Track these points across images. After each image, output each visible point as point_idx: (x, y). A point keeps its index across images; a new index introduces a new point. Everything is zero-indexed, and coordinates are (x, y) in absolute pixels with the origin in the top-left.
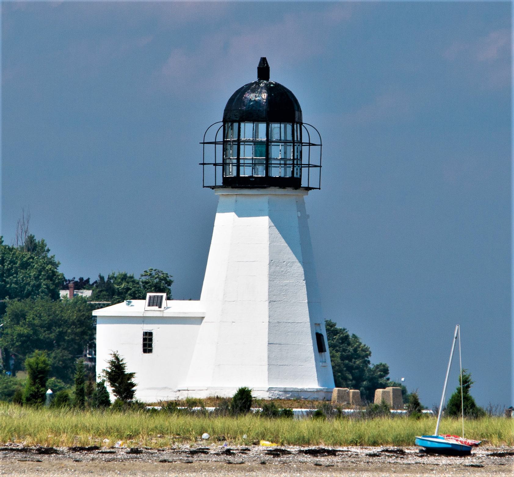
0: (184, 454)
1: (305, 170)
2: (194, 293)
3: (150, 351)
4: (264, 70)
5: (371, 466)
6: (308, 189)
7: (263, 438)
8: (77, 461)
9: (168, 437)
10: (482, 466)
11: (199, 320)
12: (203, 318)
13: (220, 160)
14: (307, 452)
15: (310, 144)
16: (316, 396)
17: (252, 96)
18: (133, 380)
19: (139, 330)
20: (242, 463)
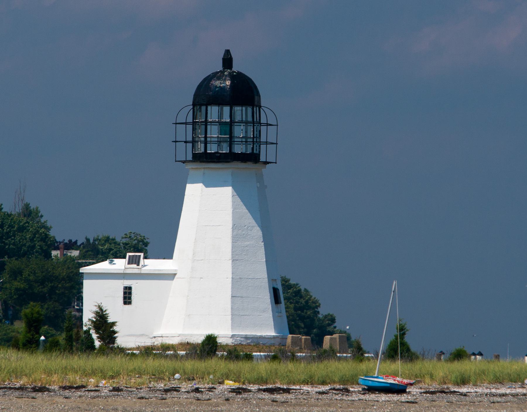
0: (159, 392)
4: (228, 61)
5: (320, 403)
6: (266, 163)
8: (66, 398)
9: (145, 377)
10: (416, 403)
11: (171, 276)
12: (175, 274)
13: (190, 139)
14: (265, 390)
15: (268, 125)
17: (217, 83)
18: (115, 328)
19: (119, 285)
20: (209, 400)
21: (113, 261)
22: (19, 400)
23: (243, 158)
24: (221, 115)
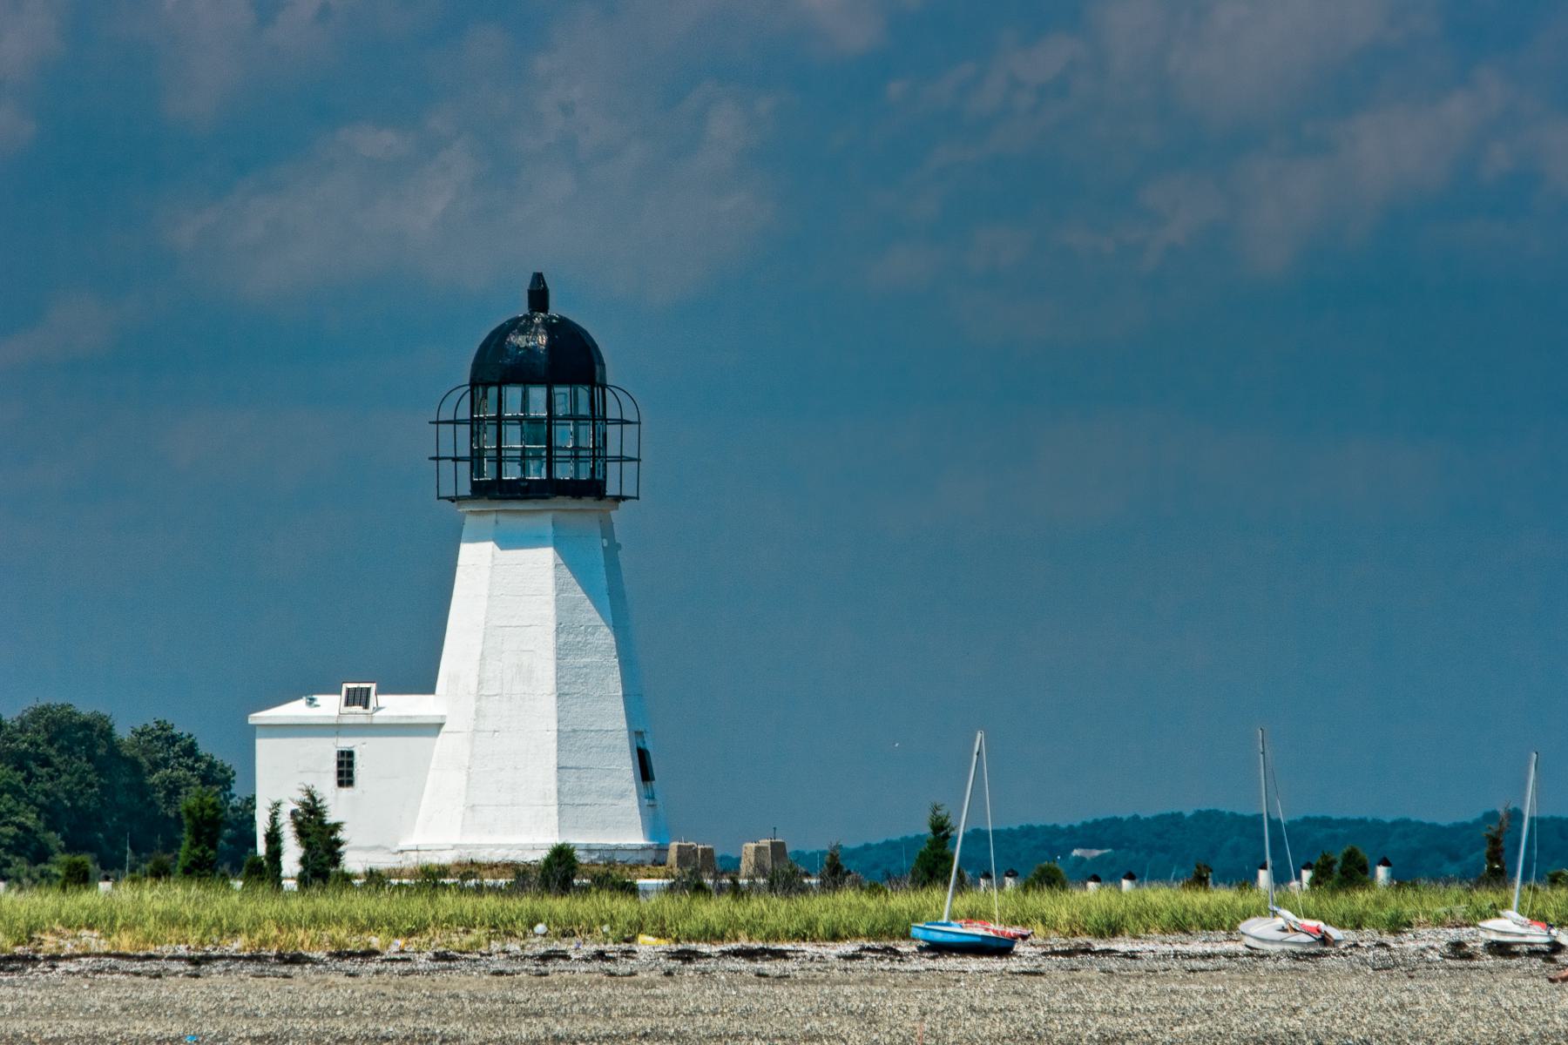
0: (528, 961)
1: (613, 468)
2: (425, 683)
3: (350, 783)
4: (539, 296)
5: (853, 977)
6: (620, 498)
7: (641, 929)
8: (351, 975)
9: (478, 933)
10: (1042, 974)
11: (433, 728)
12: (441, 725)
13: (464, 451)
14: (736, 953)
15: (622, 422)
16: (640, 857)
17: (520, 340)
18: (340, 835)
19: (326, 750)
20: (632, 974)
21: (312, 700)
22: (260, 981)
23: (575, 489)
24: (525, 406)
